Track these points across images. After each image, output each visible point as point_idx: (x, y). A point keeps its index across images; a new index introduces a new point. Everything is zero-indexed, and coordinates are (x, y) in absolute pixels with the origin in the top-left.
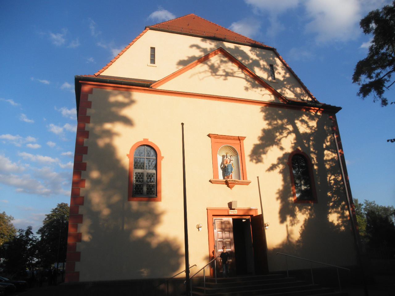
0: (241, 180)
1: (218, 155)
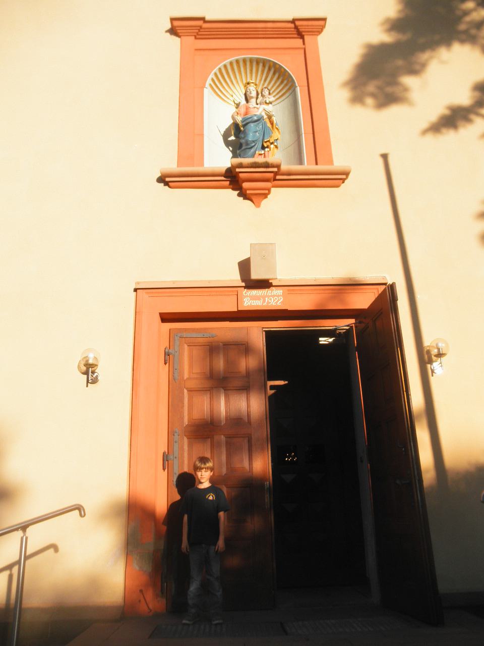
0: (308, 165)
1: (207, 92)
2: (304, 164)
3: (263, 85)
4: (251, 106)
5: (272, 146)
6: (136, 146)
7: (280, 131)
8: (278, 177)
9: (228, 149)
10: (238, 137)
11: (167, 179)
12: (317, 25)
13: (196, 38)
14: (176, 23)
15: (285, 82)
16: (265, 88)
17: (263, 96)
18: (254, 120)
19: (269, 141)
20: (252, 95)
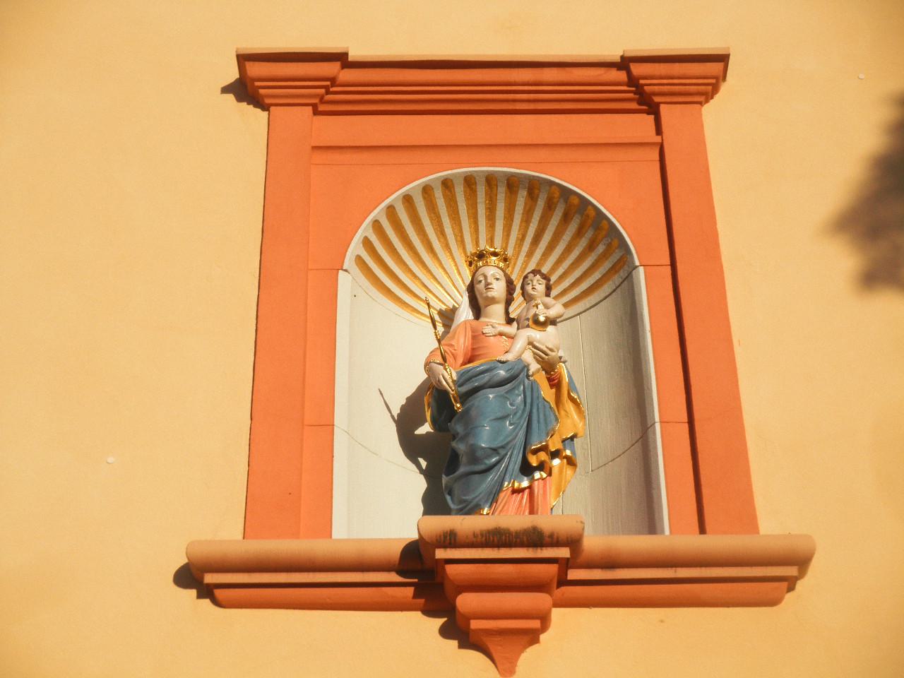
0: (675, 535)
1: (349, 283)
2: (663, 532)
3: (526, 263)
4: (488, 330)
5: (556, 462)
6: (110, 460)
7: (584, 407)
8: (573, 574)
9: (413, 467)
10: (442, 432)
11: (210, 578)
12: (702, 73)
13: (316, 112)
14: (255, 69)
15: (601, 249)
16: (535, 272)
17: (527, 297)
18: (496, 379)
19: (544, 448)
20: (490, 294)
